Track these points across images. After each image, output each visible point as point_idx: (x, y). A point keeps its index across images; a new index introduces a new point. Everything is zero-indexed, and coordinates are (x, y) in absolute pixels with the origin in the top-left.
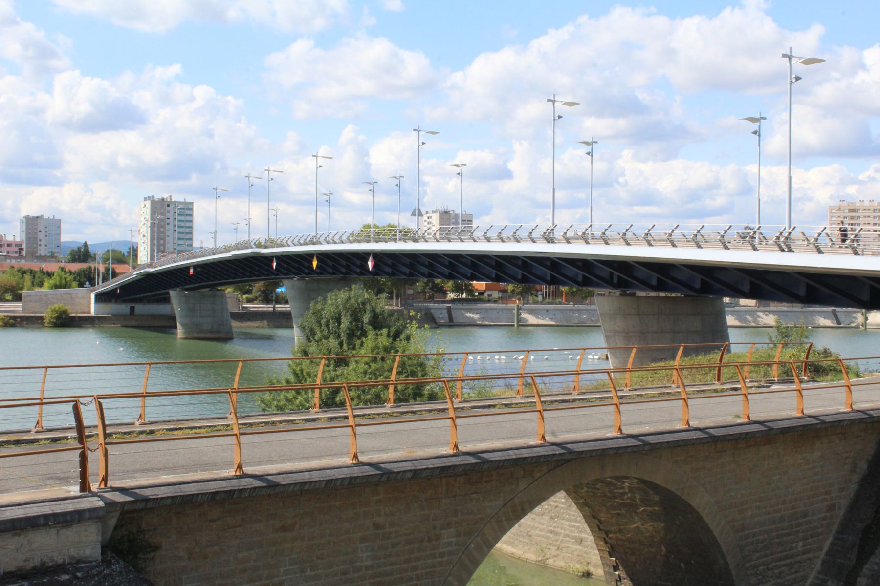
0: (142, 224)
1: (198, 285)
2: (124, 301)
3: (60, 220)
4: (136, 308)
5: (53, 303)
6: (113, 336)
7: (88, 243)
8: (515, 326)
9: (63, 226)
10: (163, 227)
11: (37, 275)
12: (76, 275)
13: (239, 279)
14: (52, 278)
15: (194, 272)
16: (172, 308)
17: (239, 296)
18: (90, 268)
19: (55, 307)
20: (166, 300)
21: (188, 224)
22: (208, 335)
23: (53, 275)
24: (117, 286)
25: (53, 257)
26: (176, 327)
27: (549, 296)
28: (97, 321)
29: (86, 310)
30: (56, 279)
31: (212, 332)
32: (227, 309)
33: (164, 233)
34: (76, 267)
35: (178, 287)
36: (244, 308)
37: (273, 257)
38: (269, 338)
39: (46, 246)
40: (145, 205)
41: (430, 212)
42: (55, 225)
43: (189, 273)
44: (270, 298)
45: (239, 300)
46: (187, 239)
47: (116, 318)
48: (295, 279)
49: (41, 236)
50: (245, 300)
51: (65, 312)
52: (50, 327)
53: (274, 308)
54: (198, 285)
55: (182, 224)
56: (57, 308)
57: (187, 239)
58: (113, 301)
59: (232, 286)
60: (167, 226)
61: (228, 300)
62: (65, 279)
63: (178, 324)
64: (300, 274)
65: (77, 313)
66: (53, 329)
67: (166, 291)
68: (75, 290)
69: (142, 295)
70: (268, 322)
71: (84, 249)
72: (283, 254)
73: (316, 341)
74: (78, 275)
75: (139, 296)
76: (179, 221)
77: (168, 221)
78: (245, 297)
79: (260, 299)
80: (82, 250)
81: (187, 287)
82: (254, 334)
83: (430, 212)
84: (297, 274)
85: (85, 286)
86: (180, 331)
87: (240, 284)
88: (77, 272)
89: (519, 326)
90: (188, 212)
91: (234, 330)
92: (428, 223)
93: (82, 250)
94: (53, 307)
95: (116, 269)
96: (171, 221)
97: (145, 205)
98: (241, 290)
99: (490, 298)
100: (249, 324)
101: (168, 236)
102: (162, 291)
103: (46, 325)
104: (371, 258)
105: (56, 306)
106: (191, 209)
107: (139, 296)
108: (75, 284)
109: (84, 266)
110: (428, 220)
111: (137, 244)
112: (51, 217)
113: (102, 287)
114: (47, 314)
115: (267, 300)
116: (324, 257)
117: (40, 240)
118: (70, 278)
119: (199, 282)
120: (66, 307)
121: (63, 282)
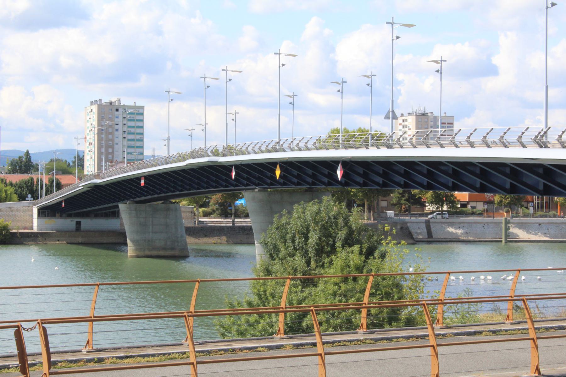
0: (88, 131)
2: (69, 216)
6: (59, 254)
8: (503, 242)
10: (111, 133)
12: (17, 188)
16: (122, 223)
17: (195, 209)
18: (32, 179)
20: (115, 214)
21: (138, 131)
22: (161, 253)
24: (61, 199)
26: (126, 244)
27: (542, 207)
28: (40, 238)
29: (28, 225)
31: (164, 249)
33: (112, 140)
34: (17, 178)
35: (128, 199)
37: (232, 166)
40: (92, 110)
41: (406, 114)
43: (140, 184)
44: (229, 211)
45: (195, 214)
47: (60, 234)
48: (256, 190)
50: (201, 214)
53: (233, 222)
55: (132, 130)
57: (138, 140)
59: (187, 198)
60: (116, 133)
61: (183, 214)
62: (6, 191)
63: (128, 241)
65: (18, 229)
68: (16, 204)
69: (89, 209)
70: (227, 237)
71: (26, 158)
73: (280, 259)
74: (20, 187)
75: (85, 210)
77: (116, 127)
78: (201, 210)
79: (218, 212)
80: (24, 160)
81: (138, 199)
83: (406, 114)
84: (258, 185)
86: (130, 248)
89: (507, 242)
91: (189, 247)
92: (404, 127)
95: (61, 181)
96: (120, 127)
97: (92, 110)
99: (474, 210)
100: (206, 240)
101: (117, 144)
102: (111, 205)
104: (340, 167)
106: (142, 114)
107: (85, 210)
108: (15, 196)
109: (25, 177)
110: (403, 124)
113: (46, 201)
115: (225, 214)
116: (287, 165)
120: (7, 223)
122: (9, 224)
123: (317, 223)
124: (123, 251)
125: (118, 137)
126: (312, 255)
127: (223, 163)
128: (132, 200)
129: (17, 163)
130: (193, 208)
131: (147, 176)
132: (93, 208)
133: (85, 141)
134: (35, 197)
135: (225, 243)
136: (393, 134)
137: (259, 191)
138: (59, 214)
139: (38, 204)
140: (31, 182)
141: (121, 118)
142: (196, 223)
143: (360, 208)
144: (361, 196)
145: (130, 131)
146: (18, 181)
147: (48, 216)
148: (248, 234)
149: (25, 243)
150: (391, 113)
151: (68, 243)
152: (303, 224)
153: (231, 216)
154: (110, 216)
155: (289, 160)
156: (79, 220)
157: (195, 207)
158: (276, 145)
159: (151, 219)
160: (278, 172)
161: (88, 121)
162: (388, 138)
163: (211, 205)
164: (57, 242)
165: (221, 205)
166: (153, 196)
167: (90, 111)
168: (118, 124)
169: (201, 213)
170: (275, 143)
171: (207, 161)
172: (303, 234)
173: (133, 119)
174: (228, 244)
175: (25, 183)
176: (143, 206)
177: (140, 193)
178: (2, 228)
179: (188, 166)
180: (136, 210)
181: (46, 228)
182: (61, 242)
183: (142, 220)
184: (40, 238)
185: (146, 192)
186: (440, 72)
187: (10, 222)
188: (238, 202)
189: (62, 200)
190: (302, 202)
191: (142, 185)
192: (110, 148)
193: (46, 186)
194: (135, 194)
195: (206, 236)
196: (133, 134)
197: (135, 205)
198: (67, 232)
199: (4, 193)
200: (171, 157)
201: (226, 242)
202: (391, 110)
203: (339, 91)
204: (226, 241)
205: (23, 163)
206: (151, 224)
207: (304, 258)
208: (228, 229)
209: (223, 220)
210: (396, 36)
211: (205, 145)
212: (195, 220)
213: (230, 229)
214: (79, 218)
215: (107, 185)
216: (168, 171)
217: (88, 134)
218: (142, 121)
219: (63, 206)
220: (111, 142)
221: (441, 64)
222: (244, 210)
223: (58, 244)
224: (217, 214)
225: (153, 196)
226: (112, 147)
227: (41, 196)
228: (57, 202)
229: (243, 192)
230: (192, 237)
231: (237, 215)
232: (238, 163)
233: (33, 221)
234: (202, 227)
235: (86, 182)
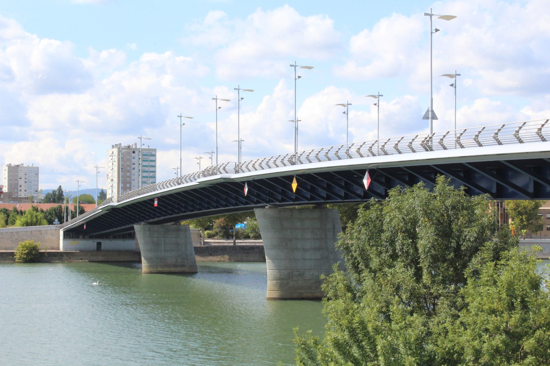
0: (110, 169)
1: (162, 218)
2: (91, 237)
3: (38, 167)
4: (102, 244)
5: (23, 240)
7: (63, 189)
9: (41, 176)
11: (11, 215)
12: (48, 214)
13: (205, 211)
14: (24, 216)
15: (158, 203)
16: (137, 244)
17: (201, 231)
18: (61, 207)
19: (26, 243)
20: (131, 236)
22: (172, 269)
23: (25, 214)
24: (83, 222)
25: (31, 199)
26: (140, 262)
28: (65, 257)
29: (55, 245)
30: (27, 217)
31: (175, 266)
32: (191, 243)
33: (130, 177)
34: (47, 207)
35: (142, 221)
36: (205, 243)
37: (244, 183)
38: (229, 272)
39: (26, 191)
40: (113, 152)
42: (34, 172)
44: (231, 234)
45: (201, 235)
46: (151, 177)
47: (83, 254)
48: (266, 207)
49: (21, 182)
50: (206, 236)
51: (35, 248)
52: (21, 262)
53: (234, 243)
54: (162, 218)
55: (146, 169)
56: (27, 245)
57: (151, 177)
58: (81, 237)
59: (195, 220)
60: (133, 171)
62: (36, 216)
63: (143, 258)
64: (273, 202)
65: (46, 249)
66: (25, 265)
67: (130, 226)
68: (46, 227)
69: (108, 231)
70: (229, 256)
71: (59, 193)
72: (256, 178)
73: (371, 271)
74: (50, 214)
75: (104, 232)
76: (144, 166)
77: (133, 166)
78: (206, 232)
79: (220, 234)
80: (57, 193)
81: (151, 220)
82: (216, 268)
85: (54, 223)
86: (144, 264)
87: (200, 219)
88: (49, 210)
90: (152, 158)
91: (197, 264)
93: (57, 193)
94: (23, 244)
95: (85, 208)
96: (136, 166)
97: (113, 152)
98: (202, 226)
100: (211, 258)
101: (134, 180)
102: (127, 226)
103: (17, 260)
104: (367, 175)
105: (27, 242)
106: (155, 155)
107: (104, 232)
108: (45, 221)
109: (56, 205)
111: (106, 190)
112: (30, 166)
113: (71, 224)
114: (18, 250)
115: (227, 236)
117: (21, 186)
118: (40, 215)
119: (164, 216)
120: (36, 244)
121: (35, 220)
122: (38, 245)
123: (426, 214)
124: (138, 268)
125: (134, 175)
126: (427, 264)
127: (235, 180)
128: (146, 221)
129: (51, 196)
130: (199, 230)
131: (160, 197)
132: (111, 230)
133: (108, 178)
134: (61, 221)
135: (228, 261)
136: (433, 135)
137: (269, 208)
138: (82, 236)
139: (64, 227)
140: (60, 210)
141: (137, 158)
142: (202, 243)
143: (486, 195)
144: (346, 220)
145: (145, 169)
146: (48, 209)
147: (73, 238)
148: (247, 253)
149: (52, 261)
150: (430, 112)
151: (90, 261)
152: (407, 218)
153: (233, 238)
154: (126, 238)
155: (307, 172)
156: (99, 241)
157: (201, 230)
158: (292, 158)
159: (163, 239)
160: (294, 186)
161: (110, 161)
162: (427, 139)
163: (215, 228)
164: (80, 261)
165: (223, 228)
166: (165, 217)
167: (112, 153)
168: (134, 164)
169: (206, 235)
170: (292, 156)
171: (219, 177)
172: (407, 231)
173: (147, 159)
174: (231, 261)
175: (55, 211)
176: (156, 227)
177: (154, 214)
178: (32, 249)
179: (200, 185)
180: (150, 230)
181: (71, 248)
182: (83, 261)
183: (155, 239)
184: (65, 257)
185: (159, 213)
186: (454, 86)
187: (39, 243)
188: (238, 226)
189: (84, 223)
190: (398, 186)
191: (155, 206)
192: (128, 183)
193: (71, 213)
194: (148, 216)
195: (211, 255)
196: (147, 172)
197: (149, 225)
198: (89, 251)
199: (35, 218)
200: (183, 177)
201: (228, 260)
202: (430, 110)
203: (344, 113)
204: (229, 259)
205: (56, 196)
206: (163, 243)
207: (411, 268)
208: (230, 248)
209: (225, 241)
210: (434, 28)
211: (217, 163)
212: (201, 241)
213: (231, 248)
214: (99, 239)
215: (123, 207)
216: (180, 192)
217: (110, 172)
218: (155, 161)
219: (85, 228)
220: (128, 179)
221: (456, 77)
222: (243, 233)
223: (81, 262)
224: (220, 236)
225: (165, 217)
226: (130, 183)
227: (67, 220)
228: (79, 225)
229: (255, 210)
230: (199, 256)
231: (238, 237)
232: (251, 179)
233: (59, 243)
234: (207, 247)
235: (104, 205)
